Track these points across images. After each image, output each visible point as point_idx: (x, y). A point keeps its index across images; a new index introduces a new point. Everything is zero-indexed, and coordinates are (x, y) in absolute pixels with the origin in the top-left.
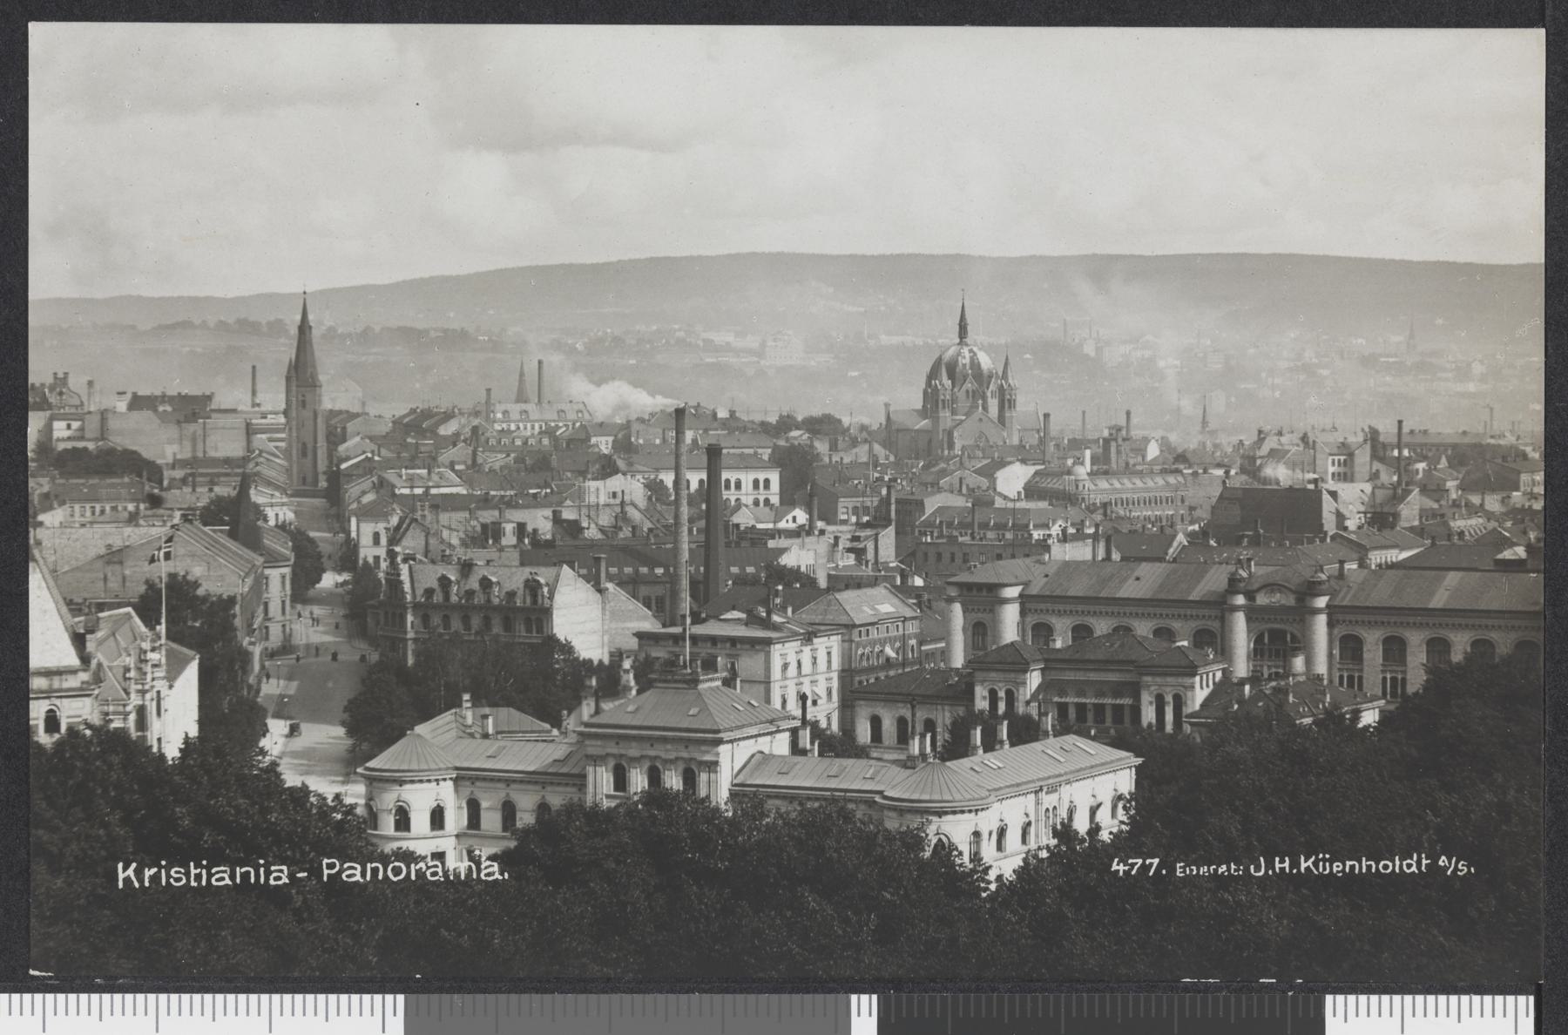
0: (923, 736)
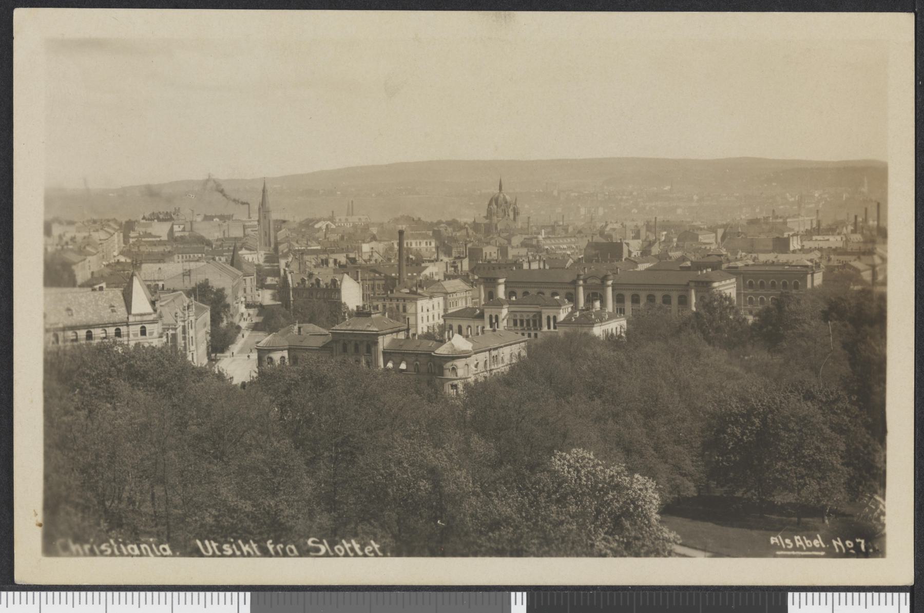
0: (449, 332)
